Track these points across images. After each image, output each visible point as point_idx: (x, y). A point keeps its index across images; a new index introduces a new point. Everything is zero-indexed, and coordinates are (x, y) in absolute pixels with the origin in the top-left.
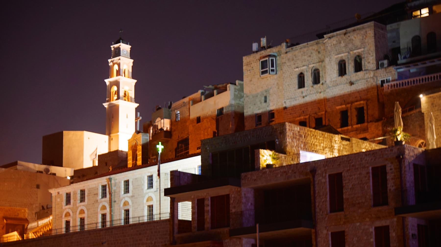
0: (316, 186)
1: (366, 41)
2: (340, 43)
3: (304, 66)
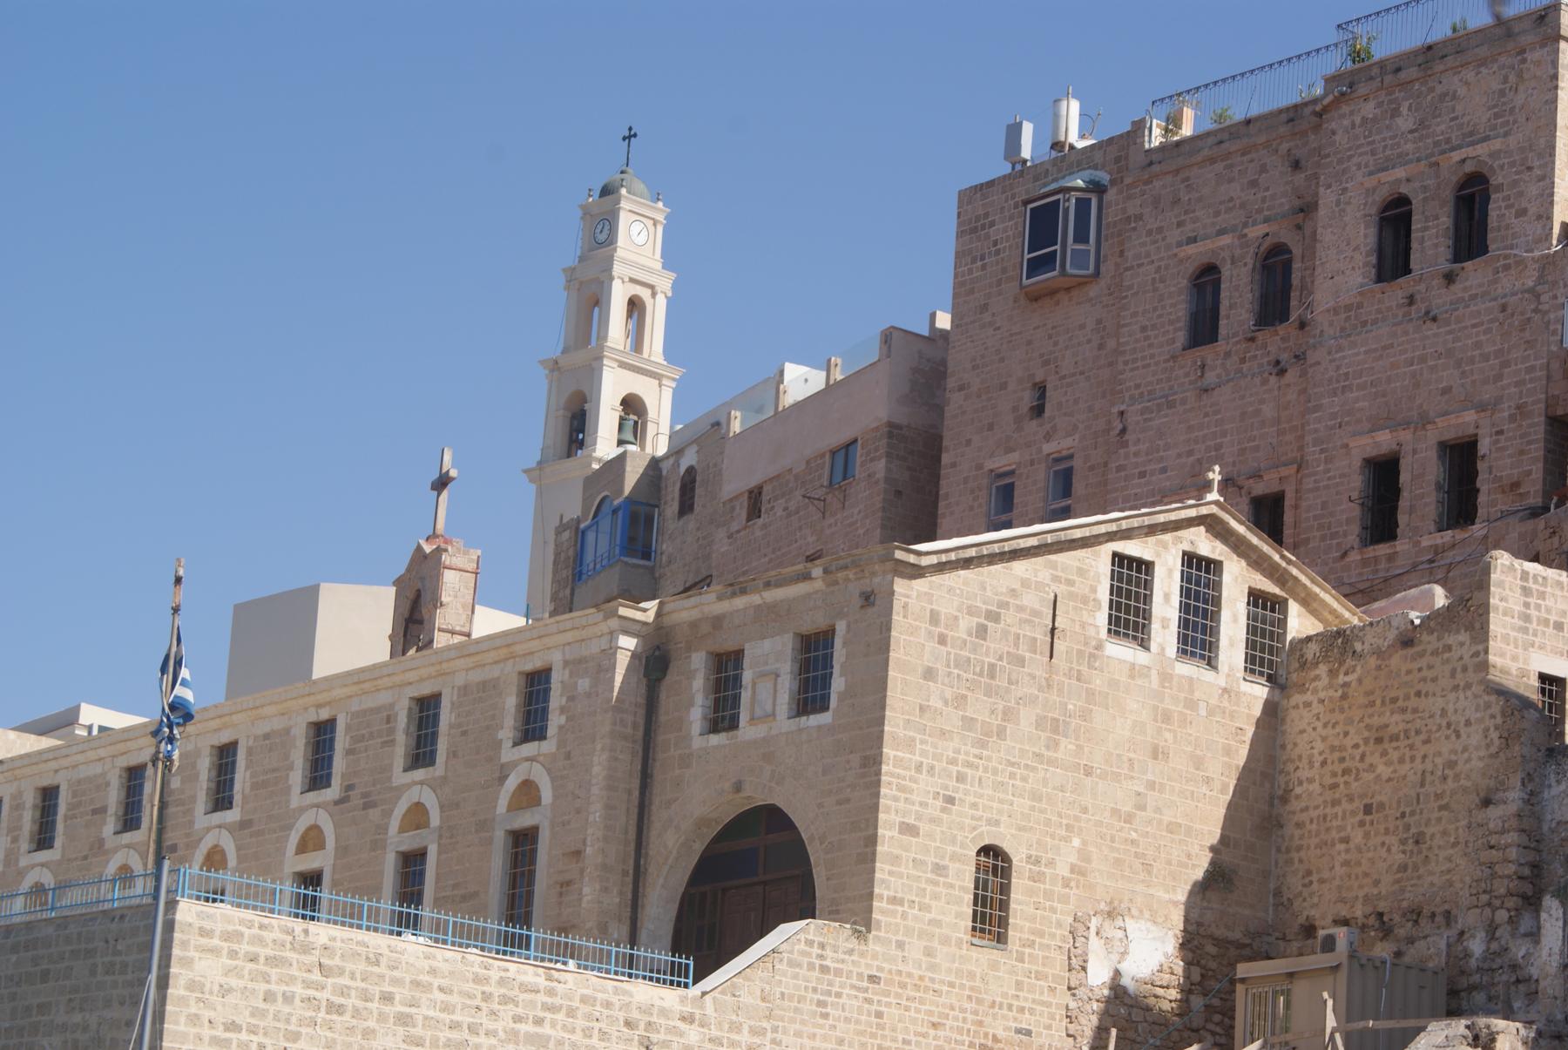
0: (1561, 938)
1: (1520, 99)
2: (1395, 113)
3: (1221, 232)
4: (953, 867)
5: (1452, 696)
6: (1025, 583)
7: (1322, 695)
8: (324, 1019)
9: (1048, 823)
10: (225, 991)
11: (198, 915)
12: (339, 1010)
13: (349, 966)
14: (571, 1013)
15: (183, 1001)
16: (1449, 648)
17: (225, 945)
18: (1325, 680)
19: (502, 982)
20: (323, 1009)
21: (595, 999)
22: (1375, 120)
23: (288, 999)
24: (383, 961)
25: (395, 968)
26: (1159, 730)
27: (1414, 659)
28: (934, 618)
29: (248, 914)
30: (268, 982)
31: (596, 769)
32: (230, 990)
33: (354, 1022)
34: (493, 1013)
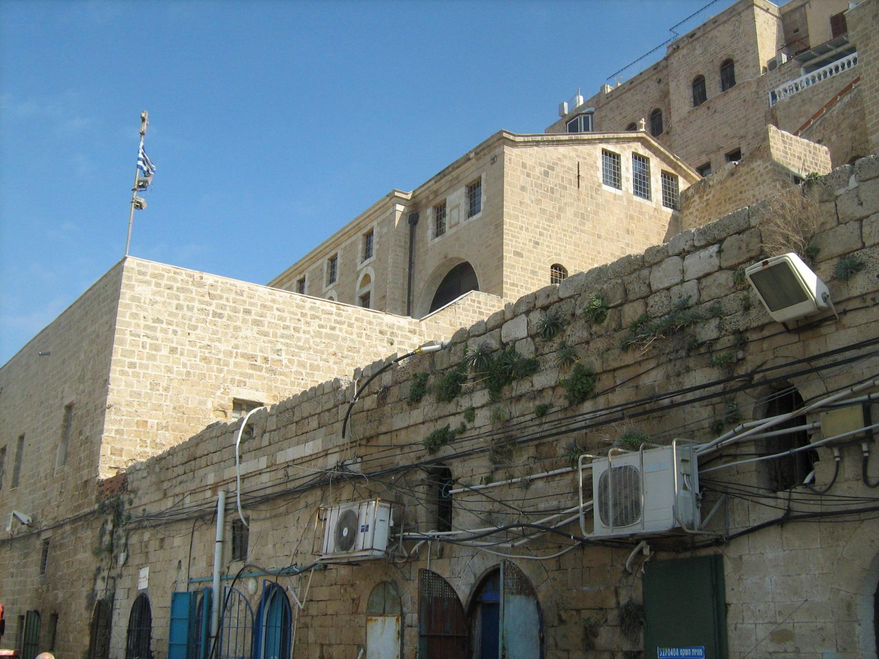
2: (695, 49)
4: (540, 272)
5: (757, 189)
6: (564, 156)
7: (697, 208)
8: (211, 320)
9: (583, 256)
10: (153, 303)
11: (138, 264)
12: (221, 316)
13: (225, 295)
14: (350, 325)
15: (128, 306)
16: (753, 169)
17: (154, 280)
18: (698, 201)
19: (312, 308)
20: (211, 315)
21: (363, 320)
22: (687, 54)
23: (190, 309)
24: (245, 294)
25: (252, 298)
26: (629, 222)
27: (737, 179)
28: (524, 166)
29: (168, 267)
30: (178, 300)
31: (390, 261)
32: (156, 302)
33: (229, 322)
34: (307, 323)
